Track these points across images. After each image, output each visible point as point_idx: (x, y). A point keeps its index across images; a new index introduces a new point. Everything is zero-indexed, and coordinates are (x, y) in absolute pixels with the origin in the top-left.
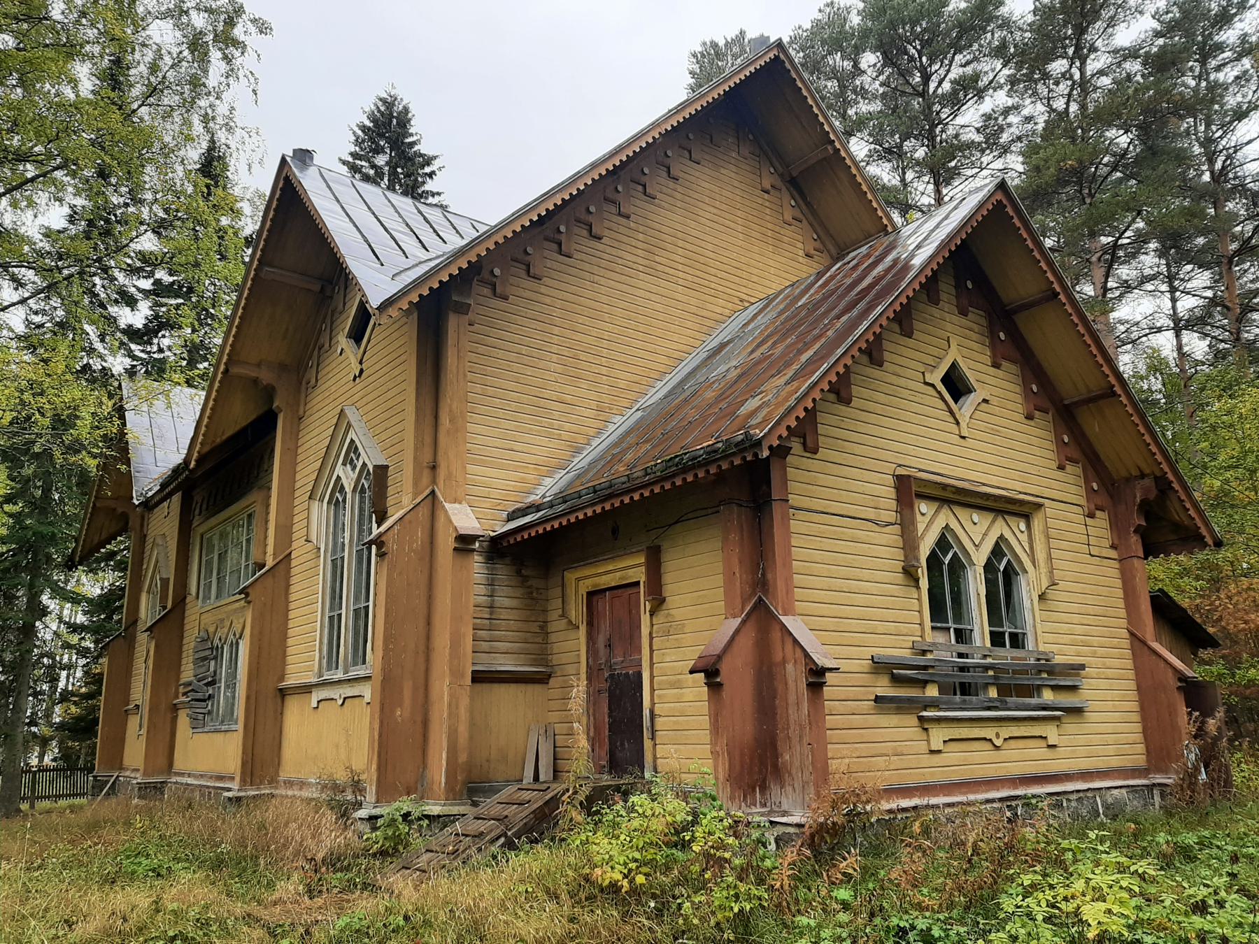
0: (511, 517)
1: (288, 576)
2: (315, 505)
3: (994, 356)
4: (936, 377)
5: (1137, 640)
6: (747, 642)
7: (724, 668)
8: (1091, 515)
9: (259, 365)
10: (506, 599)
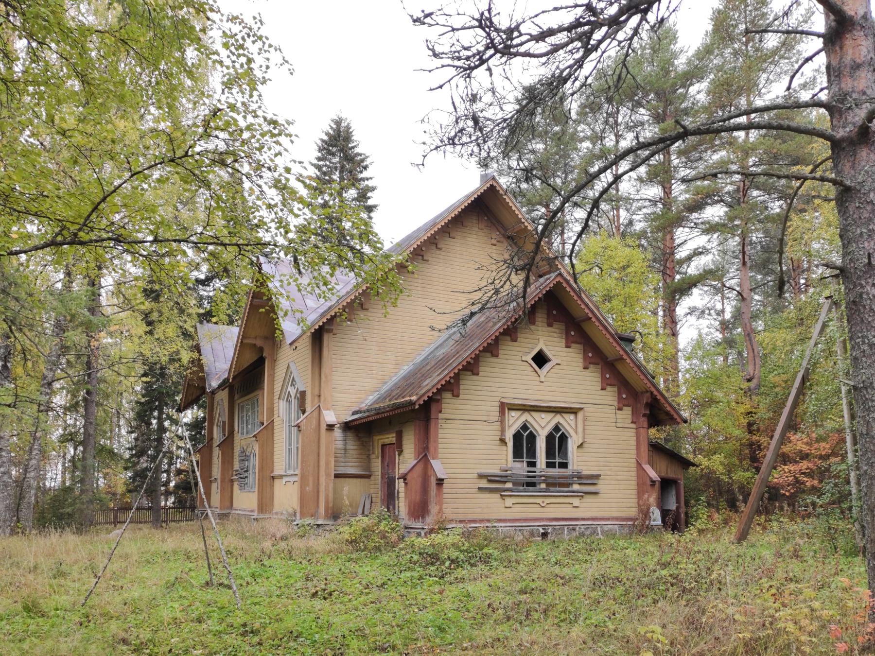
0: (354, 413)
1: (273, 429)
2: (281, 401)
3: (567, 342)
4: (529, 358)
5: (639, 465)
6: (419, 469)
7: (409, 477)
8: (620, 409)
9: (256, 338)
10: (352, 446)
